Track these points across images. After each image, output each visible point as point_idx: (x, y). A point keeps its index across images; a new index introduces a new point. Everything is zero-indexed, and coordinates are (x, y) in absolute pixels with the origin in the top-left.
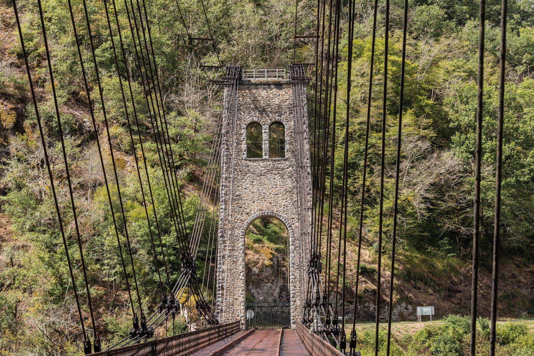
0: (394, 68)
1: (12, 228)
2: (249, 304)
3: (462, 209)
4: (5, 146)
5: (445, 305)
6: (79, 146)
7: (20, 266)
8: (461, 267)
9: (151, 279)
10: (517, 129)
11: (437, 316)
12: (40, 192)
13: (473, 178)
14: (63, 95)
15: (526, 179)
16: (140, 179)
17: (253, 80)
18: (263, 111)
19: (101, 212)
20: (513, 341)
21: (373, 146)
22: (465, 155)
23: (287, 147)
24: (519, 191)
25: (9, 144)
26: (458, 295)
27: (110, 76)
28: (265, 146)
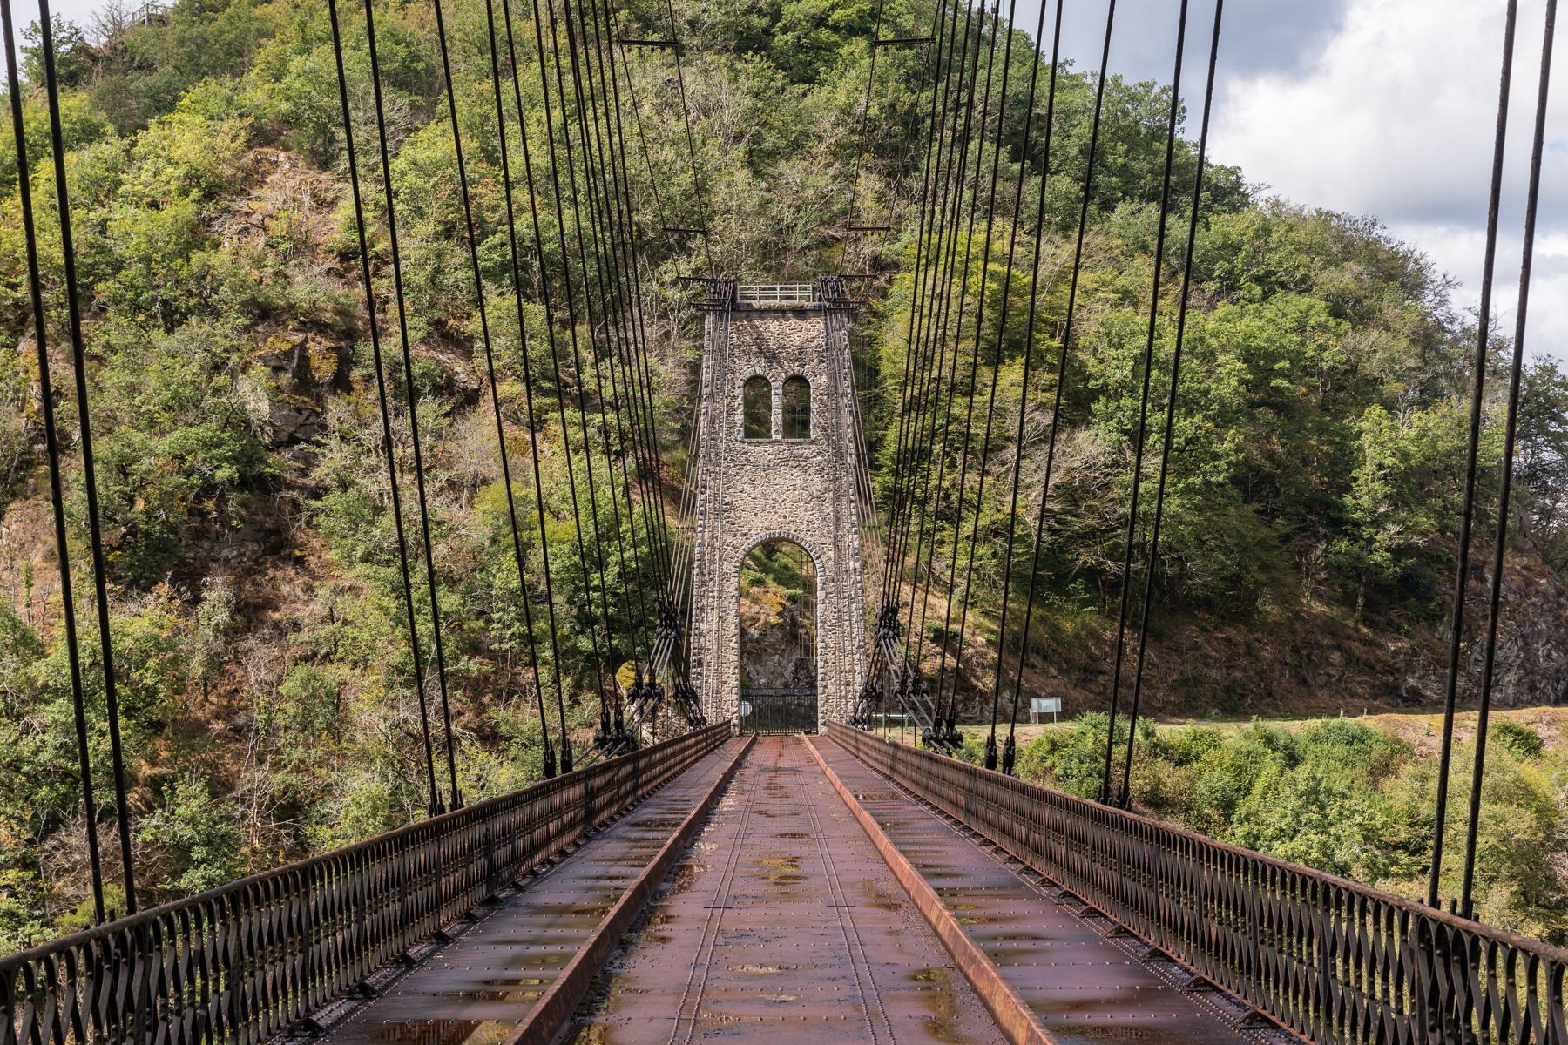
0: (994, 285)
1: (333, 555)
2: (745, 695)
3: (1110, 529)
4: (318, 415)
5: (1078, 695)
6: (447, 415)
7: (346, 623)
8: (1105, 630)
9: (574, 646)
10: (1206, 392)
11: (1066, 714)
12: (381, 495)
13: (1129, 477)
14: (418, 326)
15: (1221, 479)
16: (568, 475)
17: (756, 304)
18: (772, 357)
19: (488, 531)
20: (1197, 758)
21: (956, 419)
22: (1115, 436)
23: (814, 420)
24: (1207, 499)
25: (325, 410)
26: (1101, 679)
27: (501, 294)
28: (776, 418)
